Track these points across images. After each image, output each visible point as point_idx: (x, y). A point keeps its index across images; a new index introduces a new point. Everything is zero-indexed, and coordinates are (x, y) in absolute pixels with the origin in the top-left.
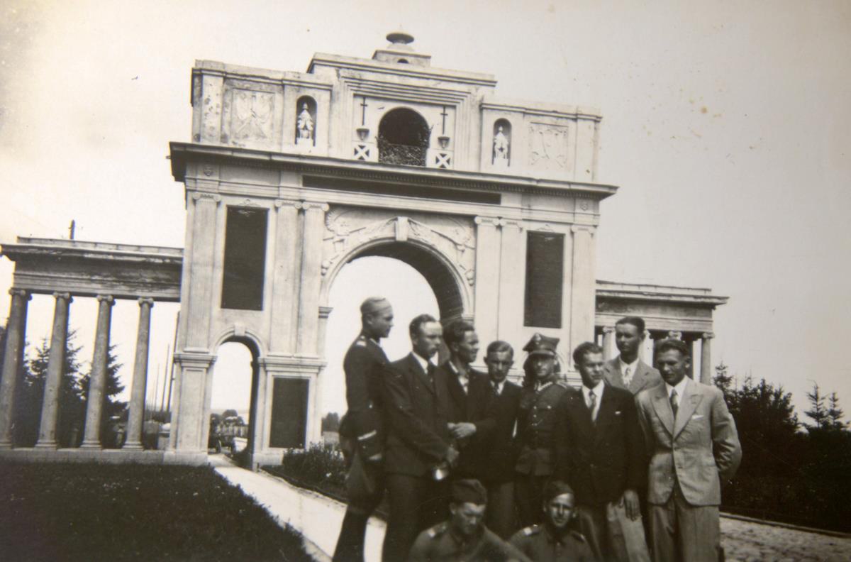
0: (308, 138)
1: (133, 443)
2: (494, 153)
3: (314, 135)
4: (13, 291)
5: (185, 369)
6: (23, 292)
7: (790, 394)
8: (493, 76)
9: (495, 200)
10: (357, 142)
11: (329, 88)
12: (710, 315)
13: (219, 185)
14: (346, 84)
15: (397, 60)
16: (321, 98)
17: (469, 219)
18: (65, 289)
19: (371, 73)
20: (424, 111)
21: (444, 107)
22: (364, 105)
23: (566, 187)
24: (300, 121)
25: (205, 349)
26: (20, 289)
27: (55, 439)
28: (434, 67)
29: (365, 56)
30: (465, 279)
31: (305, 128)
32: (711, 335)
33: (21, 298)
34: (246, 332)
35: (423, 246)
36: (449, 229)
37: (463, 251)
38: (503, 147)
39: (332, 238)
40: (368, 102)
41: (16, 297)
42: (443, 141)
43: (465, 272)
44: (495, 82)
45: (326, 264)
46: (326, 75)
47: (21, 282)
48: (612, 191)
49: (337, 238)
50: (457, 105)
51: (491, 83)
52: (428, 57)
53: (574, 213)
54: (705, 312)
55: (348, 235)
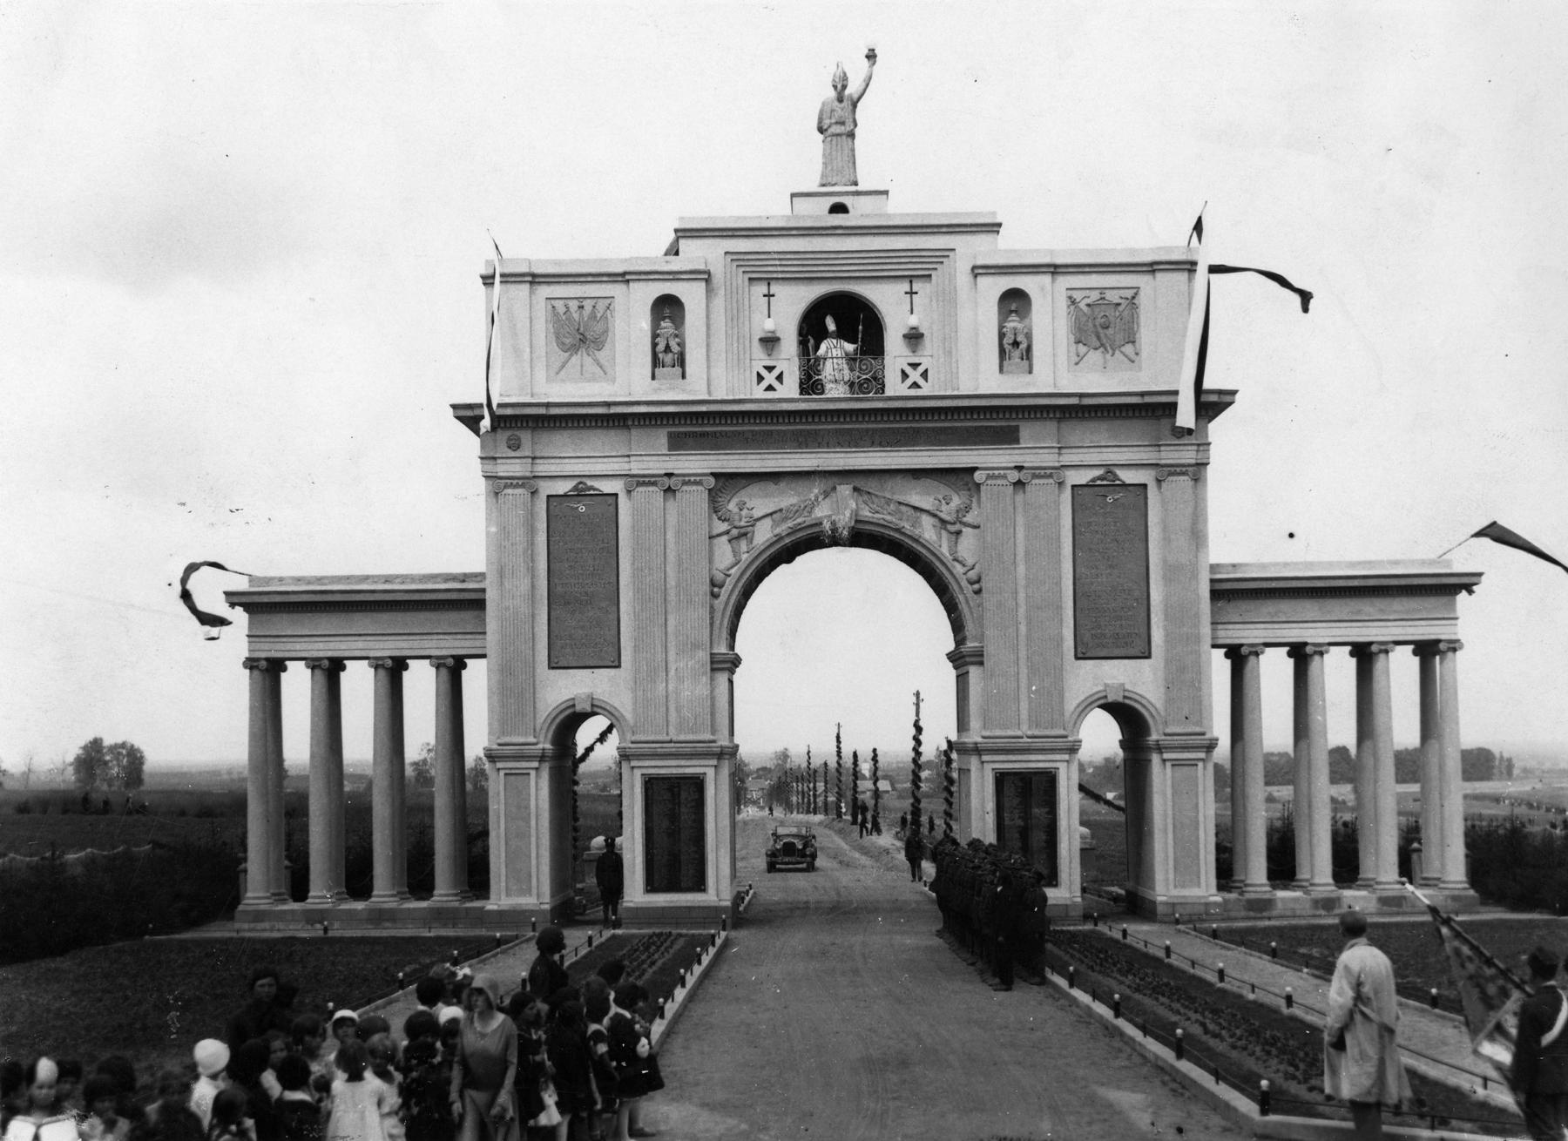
0: (674, 366)
1: (256, 895)
2: (1002, 351)
3: (681, 361)
4: (249, 663)
5: (1168, 764)
6: (450, 662)
7: (1501, 753)
8: (994, 214)
9: (1008, 437)
10: (760, 359)
11: (705, 277)
12: (1453, 606)
13: (1060, 454)
14: (735, 264)
15: (828, 206)
16: (691, 295)
17: (961, 476)
18: (321, 654)
19: (746, 240)
20: (870, 292)
21: (911, 279)
22: (769, 296)
23: (542, 411)
24: (658, 340)
25: (708, 737)
26: (258, 660)
27: (455, 887)
28: (899, 208)
29: (777, 210)
30: (964, 583)
31: (668, 349)
32: (1457, 645)
33: (267, 672)
34: (593, 705)
35: (867, 527)
36: (920, 496)
37: (959, 533)
38: (1019, 339)
39: (727, 532)
40: (774, 288)
41: (318, 672)
42: (914, 338)
43: (966, 569)
44: (1000, 225)
45: (719, 577)
46: (695, 254)
47: (478, 643)
48: (1227, 399)
49: (735, 532)
50: (933, 273)
51: (994, 228)
52: (886, 193)
53: (534, 458)
54: (1444, 600)
55: (752, 526)
